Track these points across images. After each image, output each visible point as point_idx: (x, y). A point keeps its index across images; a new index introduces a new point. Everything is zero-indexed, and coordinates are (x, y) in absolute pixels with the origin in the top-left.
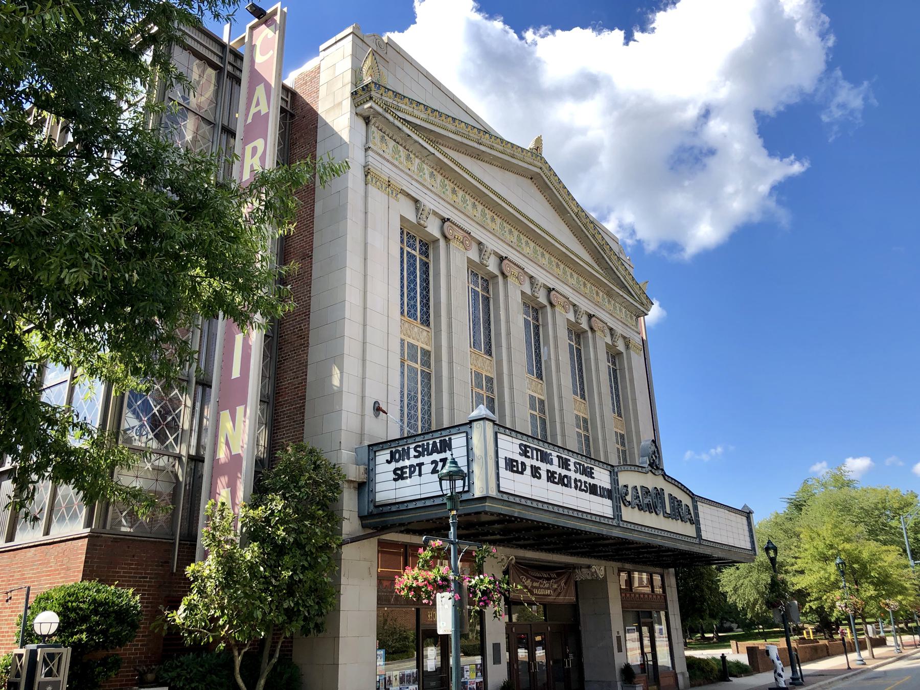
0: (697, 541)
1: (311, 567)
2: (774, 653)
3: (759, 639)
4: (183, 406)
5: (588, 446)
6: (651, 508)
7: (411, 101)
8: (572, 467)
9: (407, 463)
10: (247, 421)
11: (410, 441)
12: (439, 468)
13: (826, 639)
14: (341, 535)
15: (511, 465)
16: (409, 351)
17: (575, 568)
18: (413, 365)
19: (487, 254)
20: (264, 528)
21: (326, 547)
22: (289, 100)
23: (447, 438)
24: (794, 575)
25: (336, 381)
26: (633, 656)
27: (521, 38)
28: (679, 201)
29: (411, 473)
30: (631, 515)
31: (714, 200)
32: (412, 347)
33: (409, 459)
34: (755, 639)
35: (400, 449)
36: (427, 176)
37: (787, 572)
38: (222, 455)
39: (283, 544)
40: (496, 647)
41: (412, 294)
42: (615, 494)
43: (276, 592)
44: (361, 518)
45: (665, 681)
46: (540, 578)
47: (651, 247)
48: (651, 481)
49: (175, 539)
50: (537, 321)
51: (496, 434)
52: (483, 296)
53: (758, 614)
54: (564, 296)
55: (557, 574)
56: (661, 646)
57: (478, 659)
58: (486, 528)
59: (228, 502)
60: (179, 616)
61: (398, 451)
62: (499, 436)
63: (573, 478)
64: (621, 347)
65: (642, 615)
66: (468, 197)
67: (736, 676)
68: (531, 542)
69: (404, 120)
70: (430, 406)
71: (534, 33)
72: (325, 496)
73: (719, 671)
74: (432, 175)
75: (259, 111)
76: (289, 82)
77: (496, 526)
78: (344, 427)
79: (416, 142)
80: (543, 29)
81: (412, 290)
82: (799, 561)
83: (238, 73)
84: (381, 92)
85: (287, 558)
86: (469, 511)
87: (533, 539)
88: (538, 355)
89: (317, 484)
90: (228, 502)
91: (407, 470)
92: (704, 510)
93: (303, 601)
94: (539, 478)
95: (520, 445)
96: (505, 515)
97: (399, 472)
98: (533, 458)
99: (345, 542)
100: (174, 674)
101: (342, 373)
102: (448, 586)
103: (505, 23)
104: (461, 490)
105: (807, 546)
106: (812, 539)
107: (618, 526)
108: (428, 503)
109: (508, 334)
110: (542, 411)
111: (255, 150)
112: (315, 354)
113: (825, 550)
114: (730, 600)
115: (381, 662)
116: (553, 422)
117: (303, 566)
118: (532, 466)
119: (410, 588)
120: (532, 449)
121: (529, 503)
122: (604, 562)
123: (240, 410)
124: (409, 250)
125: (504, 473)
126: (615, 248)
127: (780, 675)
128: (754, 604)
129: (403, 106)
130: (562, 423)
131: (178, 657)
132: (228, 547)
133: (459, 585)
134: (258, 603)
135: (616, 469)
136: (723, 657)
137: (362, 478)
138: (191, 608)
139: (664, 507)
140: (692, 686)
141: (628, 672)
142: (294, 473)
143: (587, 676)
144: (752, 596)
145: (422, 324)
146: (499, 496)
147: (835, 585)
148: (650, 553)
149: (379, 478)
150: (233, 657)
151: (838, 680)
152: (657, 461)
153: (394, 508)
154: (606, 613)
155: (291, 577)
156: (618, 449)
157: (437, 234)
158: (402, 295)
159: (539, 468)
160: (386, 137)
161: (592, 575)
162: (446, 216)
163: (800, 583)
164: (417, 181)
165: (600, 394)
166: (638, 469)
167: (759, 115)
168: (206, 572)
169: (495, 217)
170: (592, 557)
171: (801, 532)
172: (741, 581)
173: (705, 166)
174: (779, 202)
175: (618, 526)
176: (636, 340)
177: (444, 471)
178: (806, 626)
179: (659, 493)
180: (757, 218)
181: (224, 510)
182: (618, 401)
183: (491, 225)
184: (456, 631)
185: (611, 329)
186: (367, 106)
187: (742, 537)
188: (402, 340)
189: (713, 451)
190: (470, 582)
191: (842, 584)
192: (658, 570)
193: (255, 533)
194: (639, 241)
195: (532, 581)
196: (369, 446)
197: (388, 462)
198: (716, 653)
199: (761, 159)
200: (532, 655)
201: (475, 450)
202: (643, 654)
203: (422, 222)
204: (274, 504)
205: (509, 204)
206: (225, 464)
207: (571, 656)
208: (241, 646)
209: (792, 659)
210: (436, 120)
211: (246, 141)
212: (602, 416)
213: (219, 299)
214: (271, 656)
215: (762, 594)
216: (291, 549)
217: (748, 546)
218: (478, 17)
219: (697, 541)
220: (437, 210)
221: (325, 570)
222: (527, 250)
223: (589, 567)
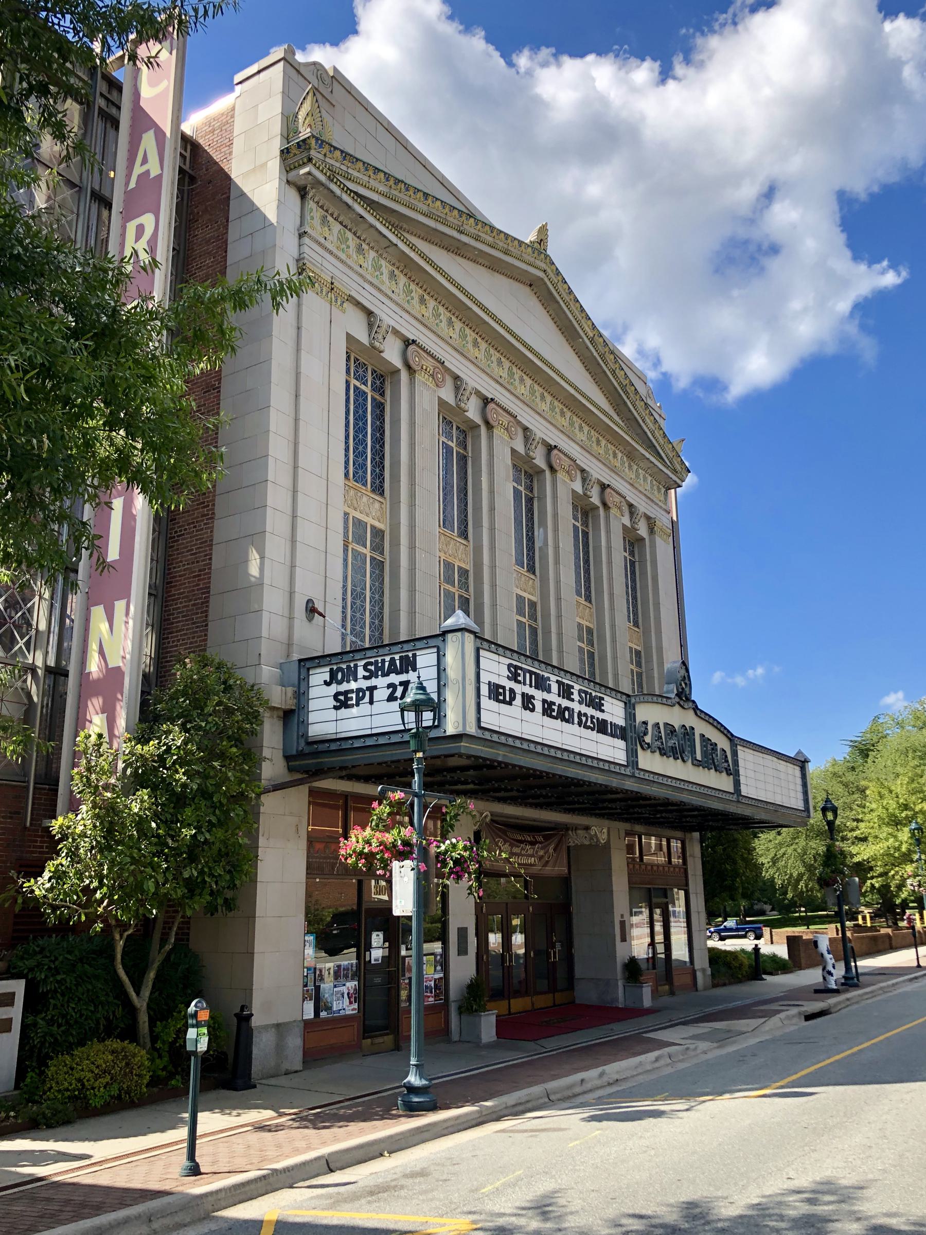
0: (734, 798)
1: (220, 824)
2: (824, 945)
3: (800, 925)
4: (37, 598)
5: (592, 665)
6: (676, 753)
7: (367, 166)
8: (576, 696)
9: (353, 685)
10: (131, 622)
11: (358, 656)
12: (398, 693)
13: (889, 927)
14: (260, 780)
15: (496, 692)
16: (356, 530)
17: (567, 829)
18: (360, 549)
19: (535, 443)
20: (156, 769)
21: (241, 797)
22: (188, 155)
23: (410, 654)
24: (853, 843)
25: (254, 569)
26: (639, 944)
27: (510, 64)
28: (725, 318)
29: (359, 700)
30: (649, 761)
31: (772, 318)
32: (359, 523)
33: (356, 680)
34: (794, 926)
35: (344, 666)
36: (385, 277)
37: (844, 839)
38: (94, 666)
39: (183, 792)
40: (462, 932)
41: (361, 448)
42: (630, 734)
43: (173, 856)
44: (288, 758)
45: (679, 980)
46: (521, 842)
47: (682, 383)
48: (678, 717)
49: (28, 782)
50: (531, 491)
51: (478, 650)
52: (458, 453)
53: (802, 892)
54: (620, 494)
55: (544, 837)
56: (678, 933)
57: (437, 947)
58: (458, 775)
59: (104, 731)
60: (40, 886)
61: (340, 669)
62: (482, 652)
63: (576, 711)
64: (643, 531)
65: (654, 894)
66: (441, 310)
67: (771, 974)
68: (515, 793)
69: (355, 193)
70: (382, 608)
71: (531, 58)
72: (239, 728)
73: (750, 966)
74: (392, 275)
75: (148, 172)
76: (187, 128)
77: (471, 772)
78: (265, 634)
79: (372, 226)
80: (545, 52)
81: (360, 442)
82: (862, 825)
83: (114, 111)
84: (324, 151)
85: (188, 811)
86: (436, 753)
87: (518, 790)
88: (531, 539)
89: (229, 711)
90: (104, 731)
91: (354, 696)
92: (745, 757)
93: (210, 868)
94: (533, 710)
95: (509, 666)
96: (485, 759)
97: (342, 698)
98: (525, 684)
99: (267, 791)
100: (31, 963)
101: (262, 558)
102: (411, 853)
103: (488, 40)
104: (430, 723)
105: (874, 806)
106: (881, 796)
107: (633, 776)
108: (382, 740)
109: (492, 509)
110: (533, 617)
111: (140, 229)
112: (223, 529)
113: (897, 811)
114: (766, 875)
115: (310, 951)
116: (547, 633)
117: (210, 821)
118: (523, 694)
119: (360, 855)
120: (525, 671)
121: (518, 744)
122: (607, 822)
123: (120, 605)
124: (358, 384)
125: (486, 702)
126: (642, 391)
127: (830, 973)
128: (798, 881)
129: (355, 174)
130: (560, 634)
131: (35, 938)
132: (109, 795)
133: (424, 851)
134: (149, 870)
135: (633, 700)
136: (756, 949)
137: (290, 704)
138: (59, 876)
139: (693, 752)
140: (715, 986)
141: (633, 968)
142: (197, 696)
143: (578, 972)
144: (796, 868)
145: (373, 491)
146: (479, 734)
147: (907, 858)
148: (671, 811)
149: (312, 705)
150: (113, 939)
151: (904, 981)
152: (687, 690)
153: (334, 747)
154: (608, 891)
155: (194, 837)
156: (632, 671)
157: (397, 362)
158: (347, 450)
159: (533, 697)
160: (330, 218)
161: (591, 839)
162: (412, 337)
163: (862, 853)
164: (371, 284)
165: (611, 595)
166: (661, 699)
167: (844, 199)
168: (80, 829)
169: (479, 340)
170: (592, 815)
171: (866, 788)
172: (783, 850)
173: (763, 269)
174: (863, 327)
175: (633, 776)
176: (663, 521)
177: (408, 700)
178: (862, 908)
179: (688, 733)
180: (831, 349)
181: (101, 744)
182: (635, 606)
183: (473, 352)
184: (418, 912)
185: (631, 506)
186: (303, 171)
187: (792, 794)
188: (346, 514)
189: (750, 672)
190: (439, 847)
191: (915, 857)
192: (679, 834)
193: (142, 776)
194: (664, 374)
195: (512, 845)
196: (300, 661)
197: (327, 684)
198: (747, 944)
199: (842, 263)
200: (507, 942)
201: (449, 671)
202: (652, 944)
203: (377, 344)
204: (171, 737)
205: (499, 322)
206: (99, 680)
207: (558, 947)
208: (123, 926)
209: (846, 952)
210: (401, 195)
211: (128, 216)
212: (613, 626)
213: (123, 462)
214: (164, 940)
215: (810, 868)
216: (193, 799)
217: (800, 805)
218: (450, 29)
219: (734, 798)
220: (398, 327)
221: (239, 828)
222: (521, 390)
223: (587, 828)
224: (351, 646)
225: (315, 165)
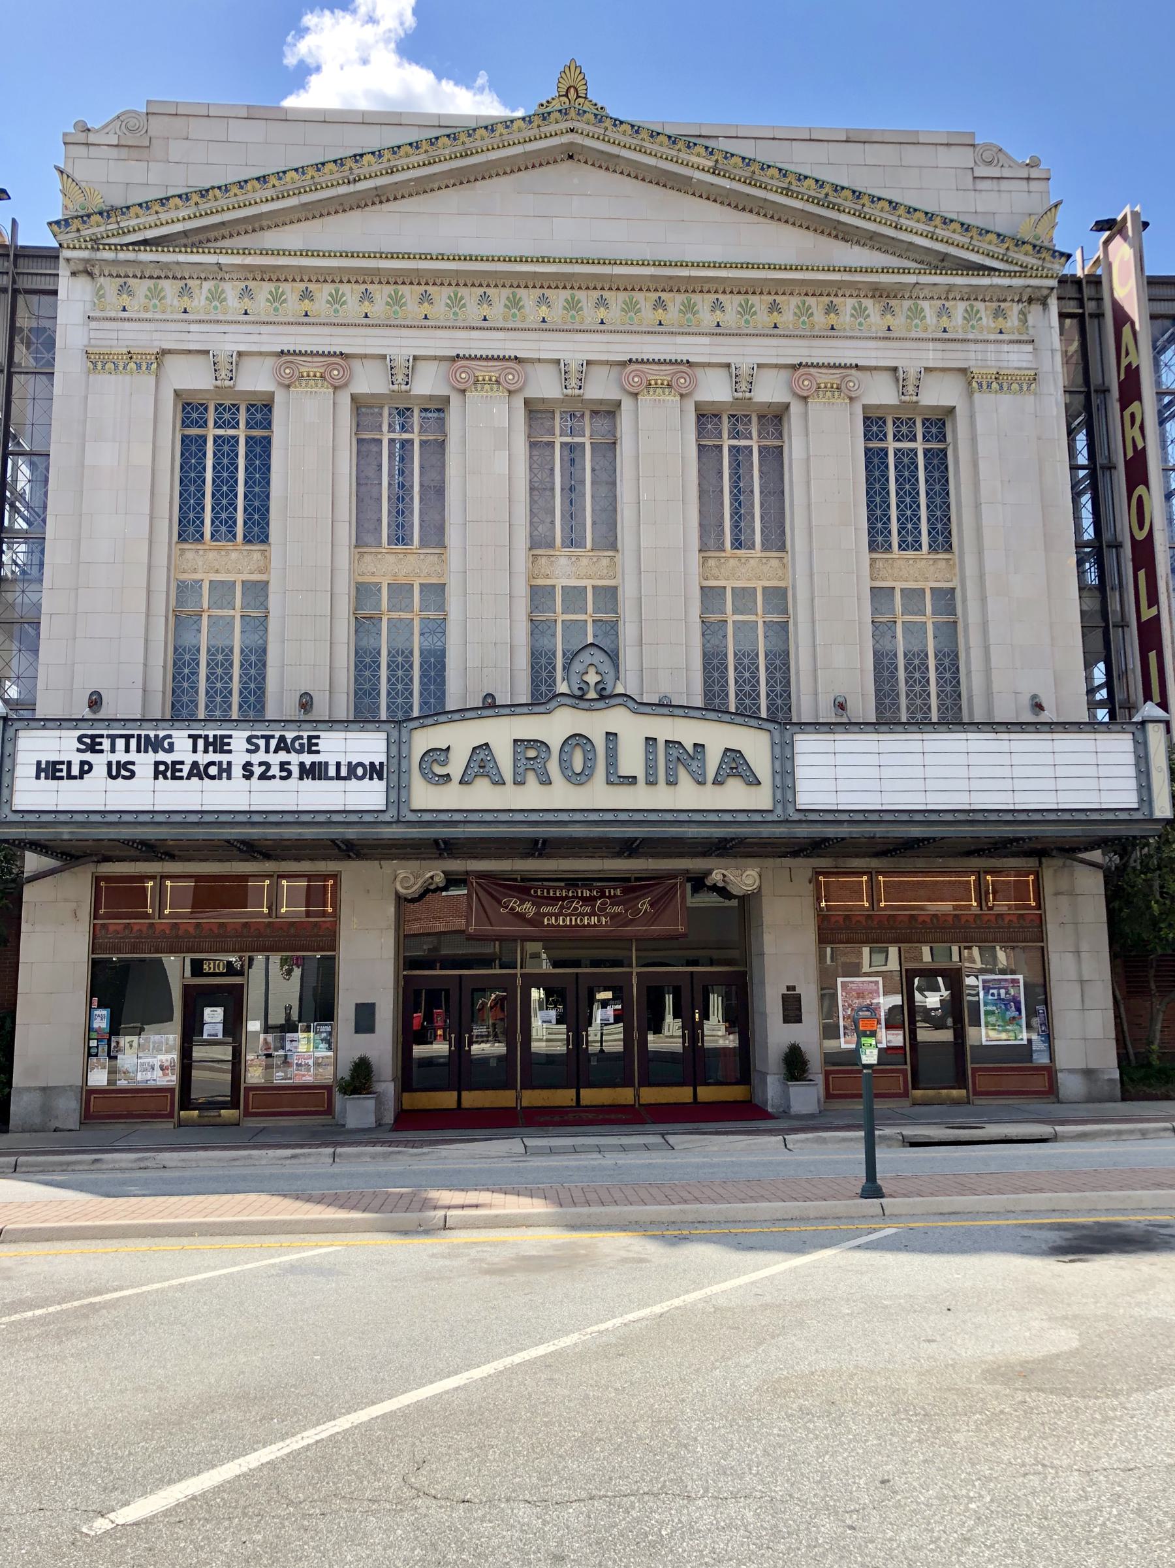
7: (145, 206)
69: (132, 244)
84: (74, 228)
224: (421, 709)
225: (68, 247)
